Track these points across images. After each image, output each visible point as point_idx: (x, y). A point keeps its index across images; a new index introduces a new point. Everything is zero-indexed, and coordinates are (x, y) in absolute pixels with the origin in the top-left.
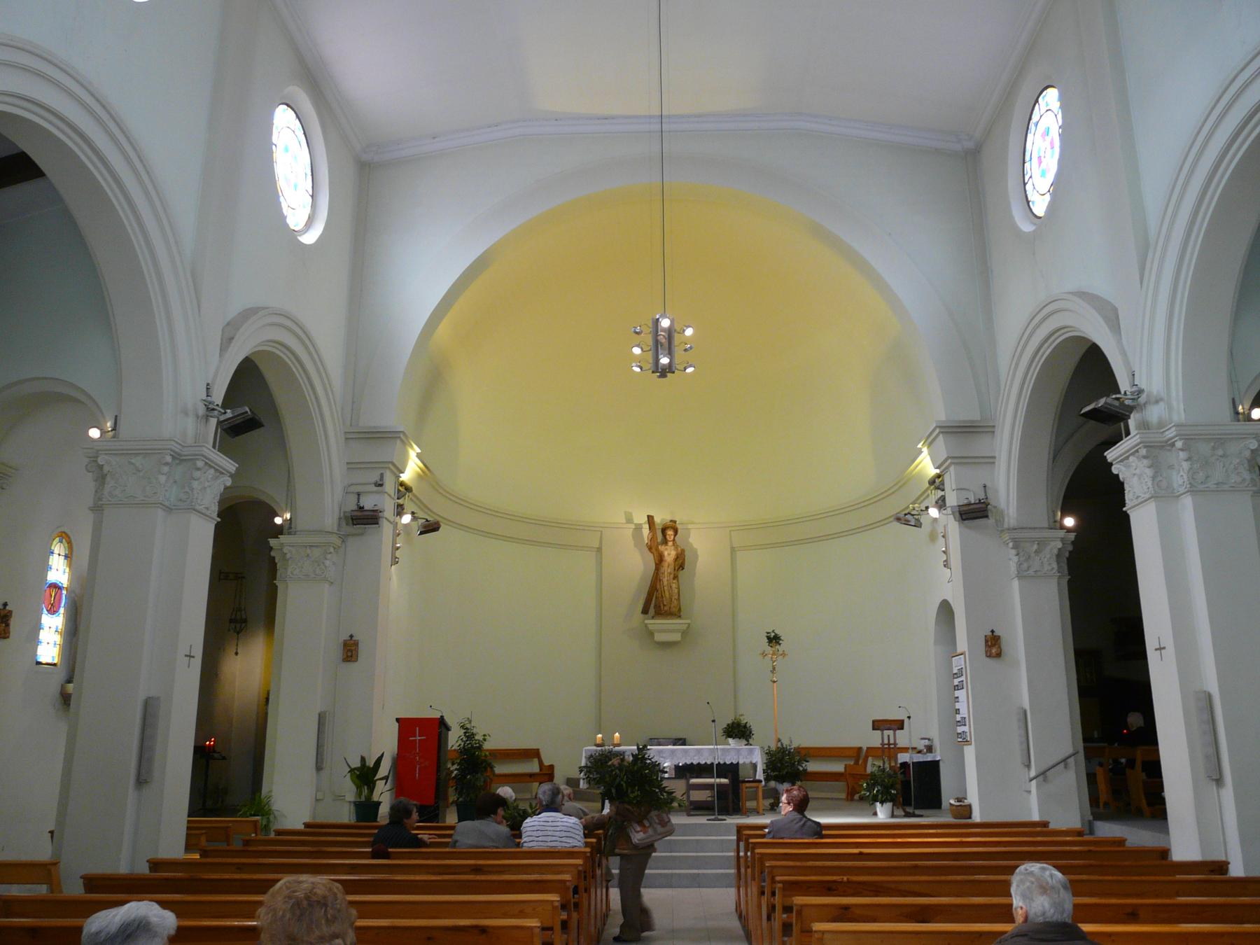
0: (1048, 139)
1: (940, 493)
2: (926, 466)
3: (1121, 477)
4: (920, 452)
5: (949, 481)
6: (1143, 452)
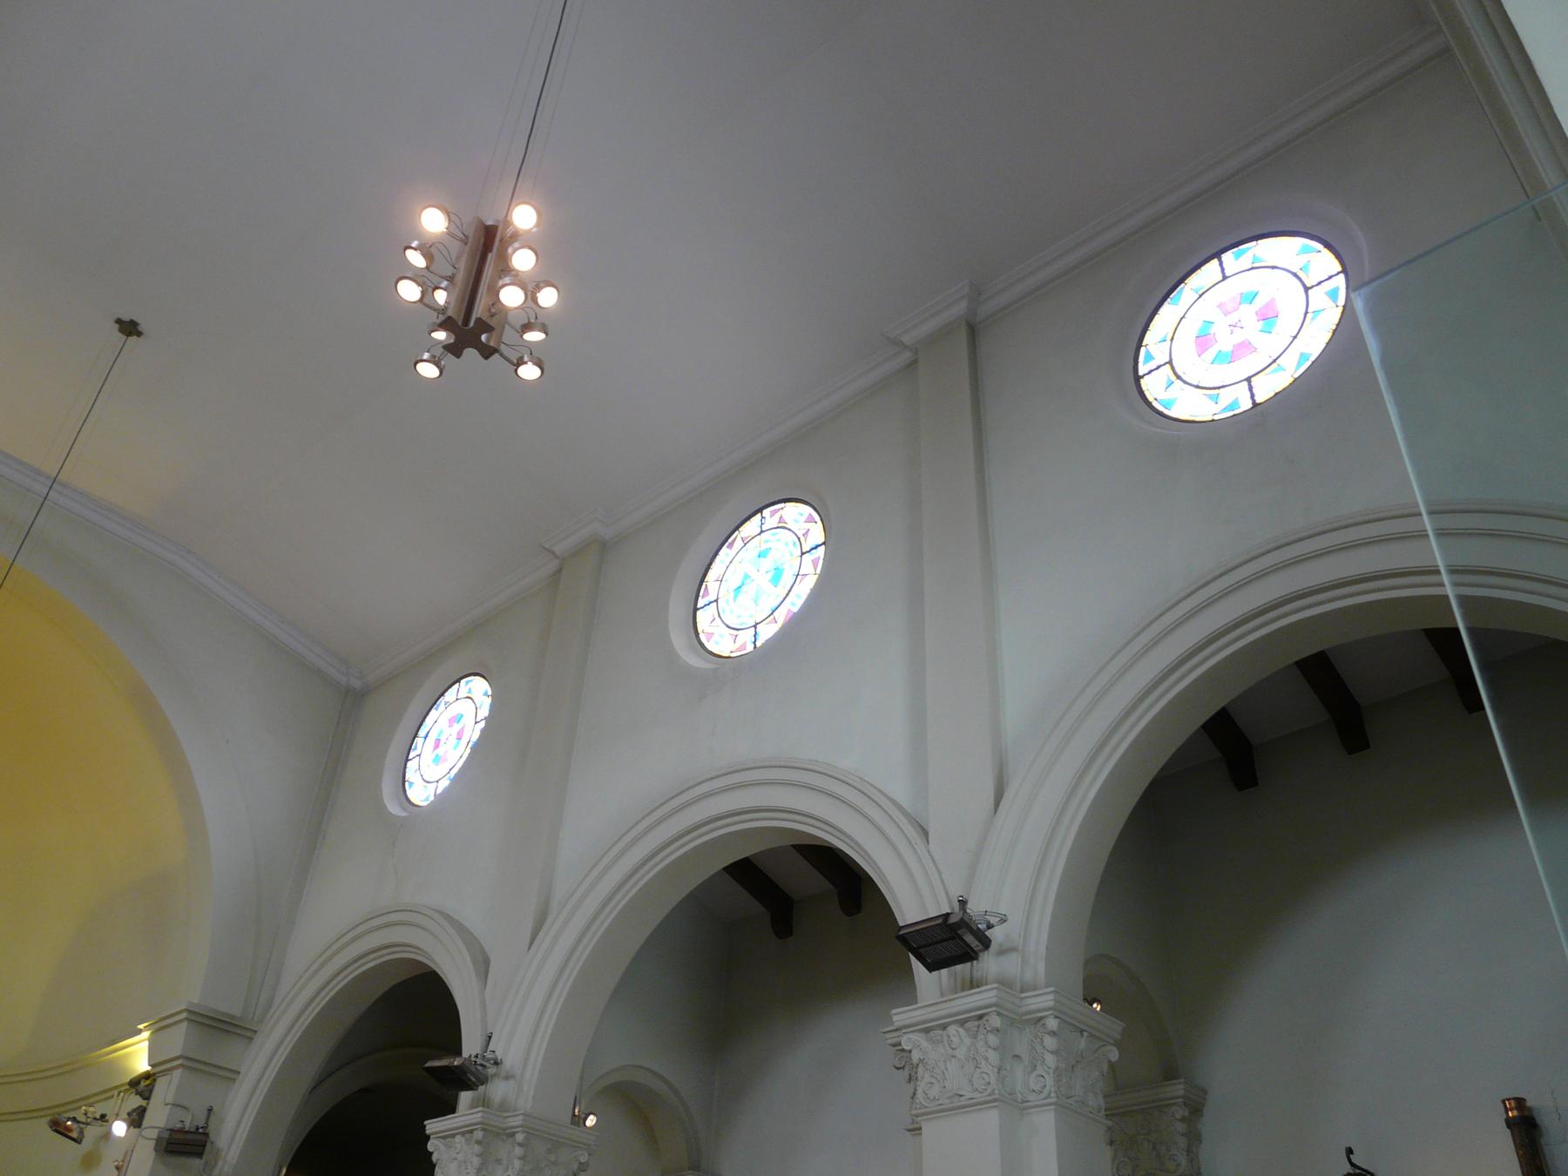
0: (457, 727)
1: (144, 1103)
2: (137, 1055)
3: (434, 1158)
4: (140, 1032)
5: (164, 1091)
6: (479, 1135)
